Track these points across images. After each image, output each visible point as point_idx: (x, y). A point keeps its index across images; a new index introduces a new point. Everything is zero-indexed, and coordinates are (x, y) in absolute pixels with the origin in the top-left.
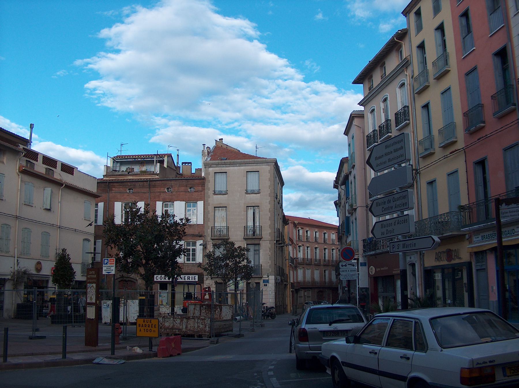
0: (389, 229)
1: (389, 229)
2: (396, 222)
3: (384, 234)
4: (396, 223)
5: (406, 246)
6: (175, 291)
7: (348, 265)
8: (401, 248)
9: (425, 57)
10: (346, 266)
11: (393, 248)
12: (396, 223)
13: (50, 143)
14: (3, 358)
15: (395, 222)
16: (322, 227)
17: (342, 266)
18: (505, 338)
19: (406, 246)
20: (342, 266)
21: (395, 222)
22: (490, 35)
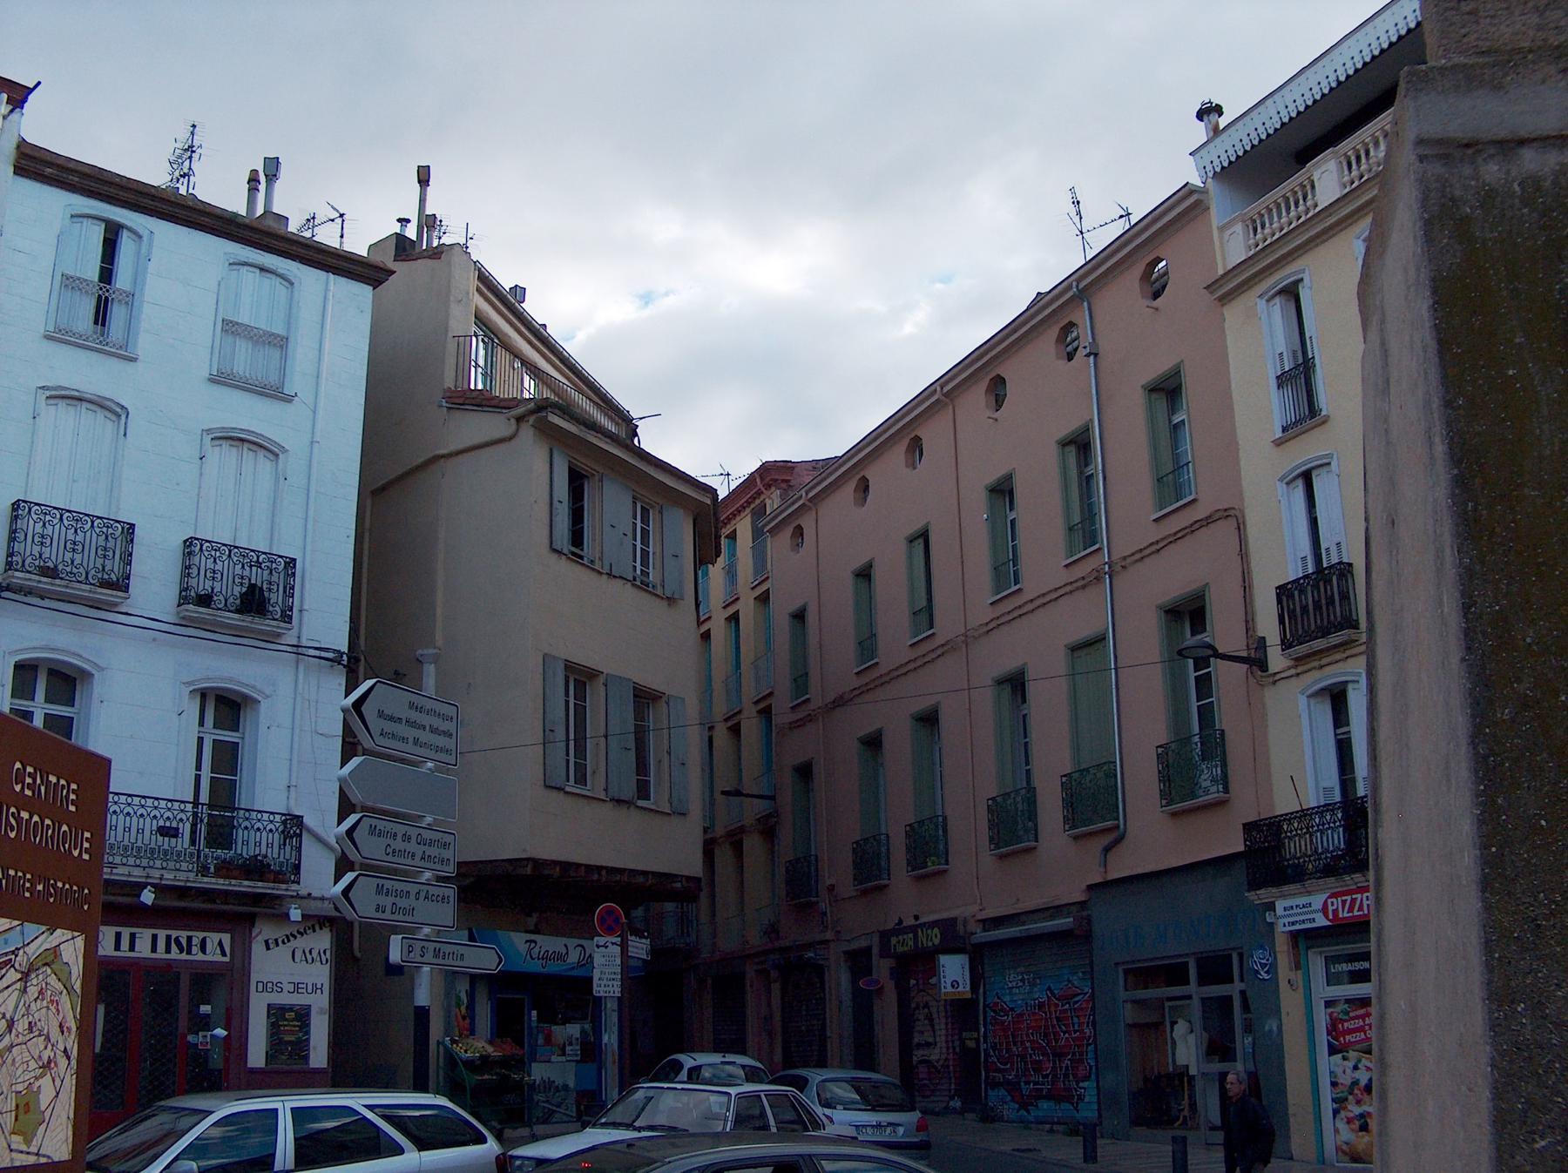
0: (402, 903)
1: (402, 903)
2: (423, 895)
3: (383, 912)
4: (422, 897)
5: (441, 954)
6: (234, 809)
7: (610, 945)
8: (429, 957)
9: (1013, 522)
10: (606, 947)
11: (410, 952)
12: (422, 897)
13: (465, 1001)
14: (1222, 1148)
15: (418, 893)
16: (267, 271)
17: (598, 946)
18: (175, 1139)
19: (441, 954)
20: (598, 946)
21: (418, 893)
22: (859, 669)
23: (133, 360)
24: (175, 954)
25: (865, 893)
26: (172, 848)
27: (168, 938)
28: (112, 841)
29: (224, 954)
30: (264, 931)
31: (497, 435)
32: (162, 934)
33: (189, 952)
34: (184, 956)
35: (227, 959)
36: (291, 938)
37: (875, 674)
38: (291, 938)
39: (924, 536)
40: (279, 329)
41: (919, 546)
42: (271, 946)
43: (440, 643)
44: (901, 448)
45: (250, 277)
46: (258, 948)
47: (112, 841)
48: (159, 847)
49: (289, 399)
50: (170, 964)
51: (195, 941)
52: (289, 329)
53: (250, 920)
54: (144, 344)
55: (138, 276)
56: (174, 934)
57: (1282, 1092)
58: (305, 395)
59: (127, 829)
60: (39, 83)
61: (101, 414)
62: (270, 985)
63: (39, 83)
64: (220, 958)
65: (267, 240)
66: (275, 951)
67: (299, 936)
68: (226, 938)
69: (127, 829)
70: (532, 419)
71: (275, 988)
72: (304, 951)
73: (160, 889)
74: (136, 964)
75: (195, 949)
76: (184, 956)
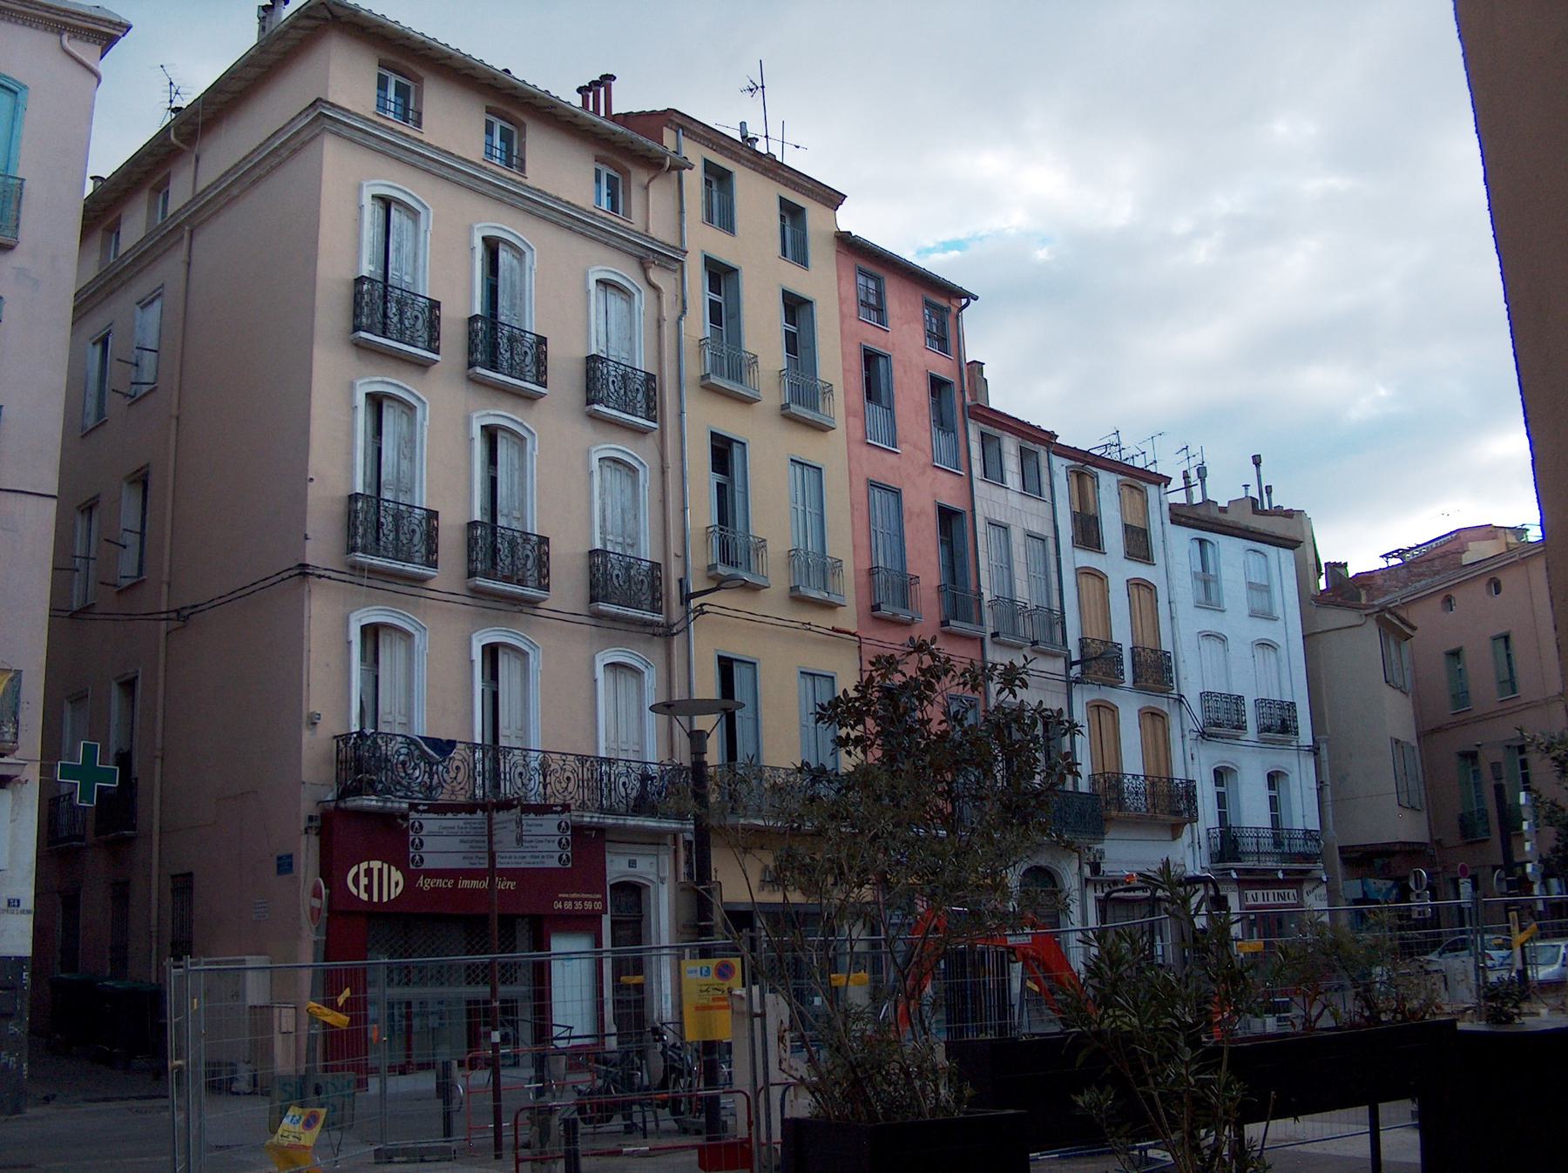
23: (1223, 611)
25: (376, 1163)
30: (1307, 887)
31: (1355, 623)
32: (1276, 891)
37: (1518, 702)
39: (801, 672)
40: (1265, 583)
41: (1501, 643)
43: (1329, 732)
44: (1439, 598)
45: (1251, 555)
49: (1276, 619)
52: (1269, 582)
53: (1301, 882)
54: (1226, 604)
55: (1217, 569)
56: (1280, 891)
58: (1281, 617)
61: (1218, 640)
65: (1280, 541)
68: (1295, 891)
70: (1375, 616)
73: (1284, 871)
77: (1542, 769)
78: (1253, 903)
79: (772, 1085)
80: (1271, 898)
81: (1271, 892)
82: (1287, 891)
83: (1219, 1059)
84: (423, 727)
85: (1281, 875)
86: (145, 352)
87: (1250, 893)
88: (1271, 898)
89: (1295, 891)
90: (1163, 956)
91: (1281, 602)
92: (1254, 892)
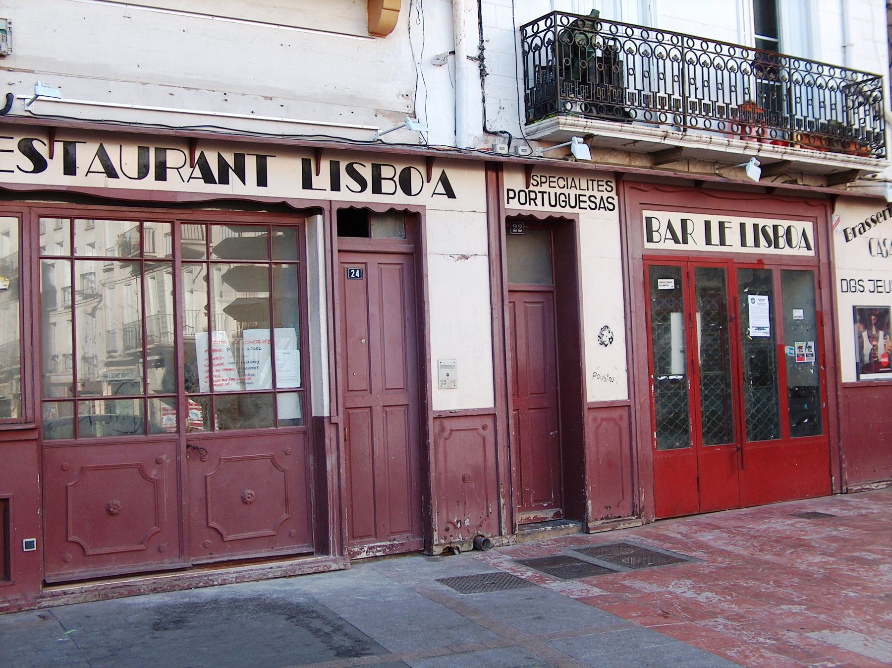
24: (764, 249)
26: (655, 94)
27: (756, 226)
28: (631, 90)
29: (809, 248)
32: (749, 222)
33: (777, 246)
34: (772, 251)
35: (812, 253)
36: (867, 227)
38: (867, 227)
42: (850, 236)
46: (838, 238)
47: (631, 90)
48: (640, 91)
50: (760, 261)
51: (781, 232)
53: (830, 201)
56: (761, 222)
57: (777, 159)
59: (706, 84)
60: (86, 175)
62: (853, 283)
63: (86, 175)
64: (804, 252)
66: (854, 241)
67: (872, 224)
68: (808, 226)
69: (706, 84)
71: (858, 287)
72: (879, 243)
74: (728, 260)
75: (782, 241)
76: (772, 251)
77: (888, 243)
78: (670, 245)
79: (121, 146)
80: (734, 236)
81: (733, 223)
82: (784, 224)
83: (217, 182)
84: (139, 335)
85: (753, 173)
86: (393, 127)
87: (662, 218)
88: (734, 236)
89: (808, 226)
90: (304, 393)
91: (206, 347)
92: (676, 218)
